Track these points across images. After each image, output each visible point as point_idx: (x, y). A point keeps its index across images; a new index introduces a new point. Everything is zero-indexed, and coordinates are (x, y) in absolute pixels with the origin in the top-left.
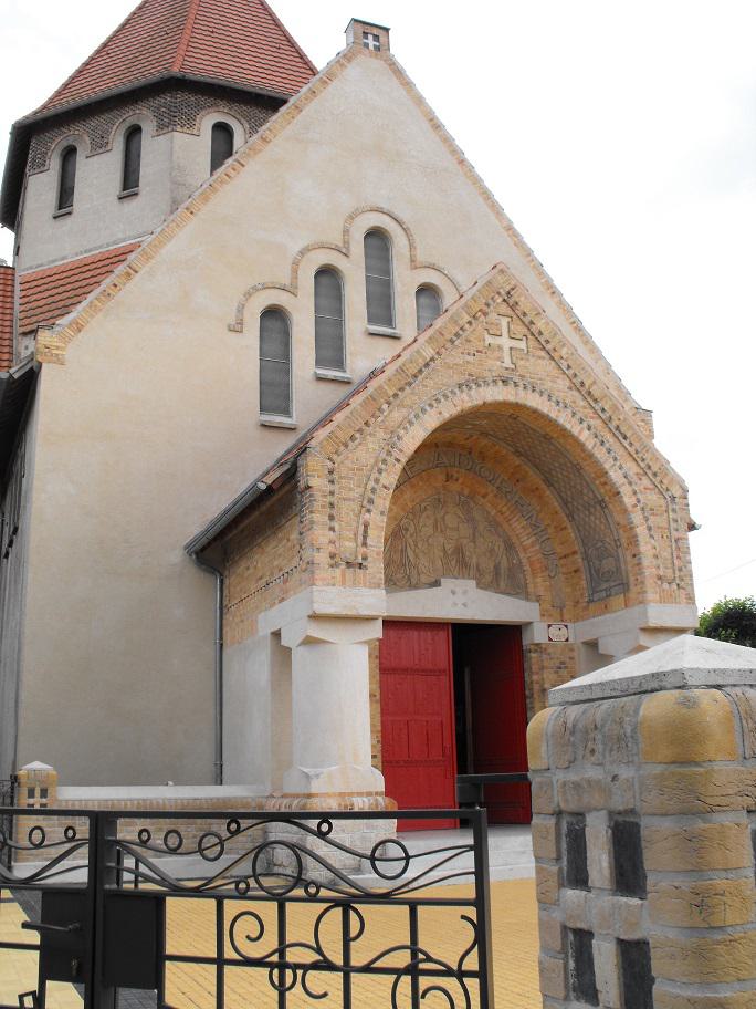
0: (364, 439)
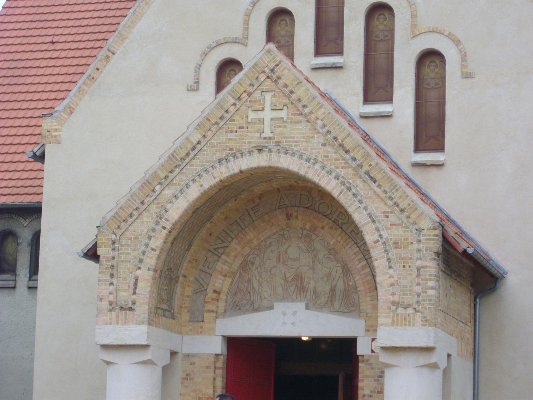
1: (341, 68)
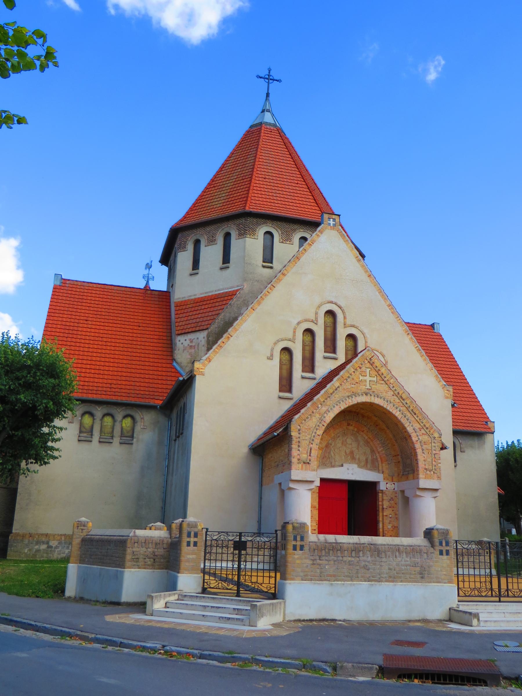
0: (311, 418)
1: (337, 359)
